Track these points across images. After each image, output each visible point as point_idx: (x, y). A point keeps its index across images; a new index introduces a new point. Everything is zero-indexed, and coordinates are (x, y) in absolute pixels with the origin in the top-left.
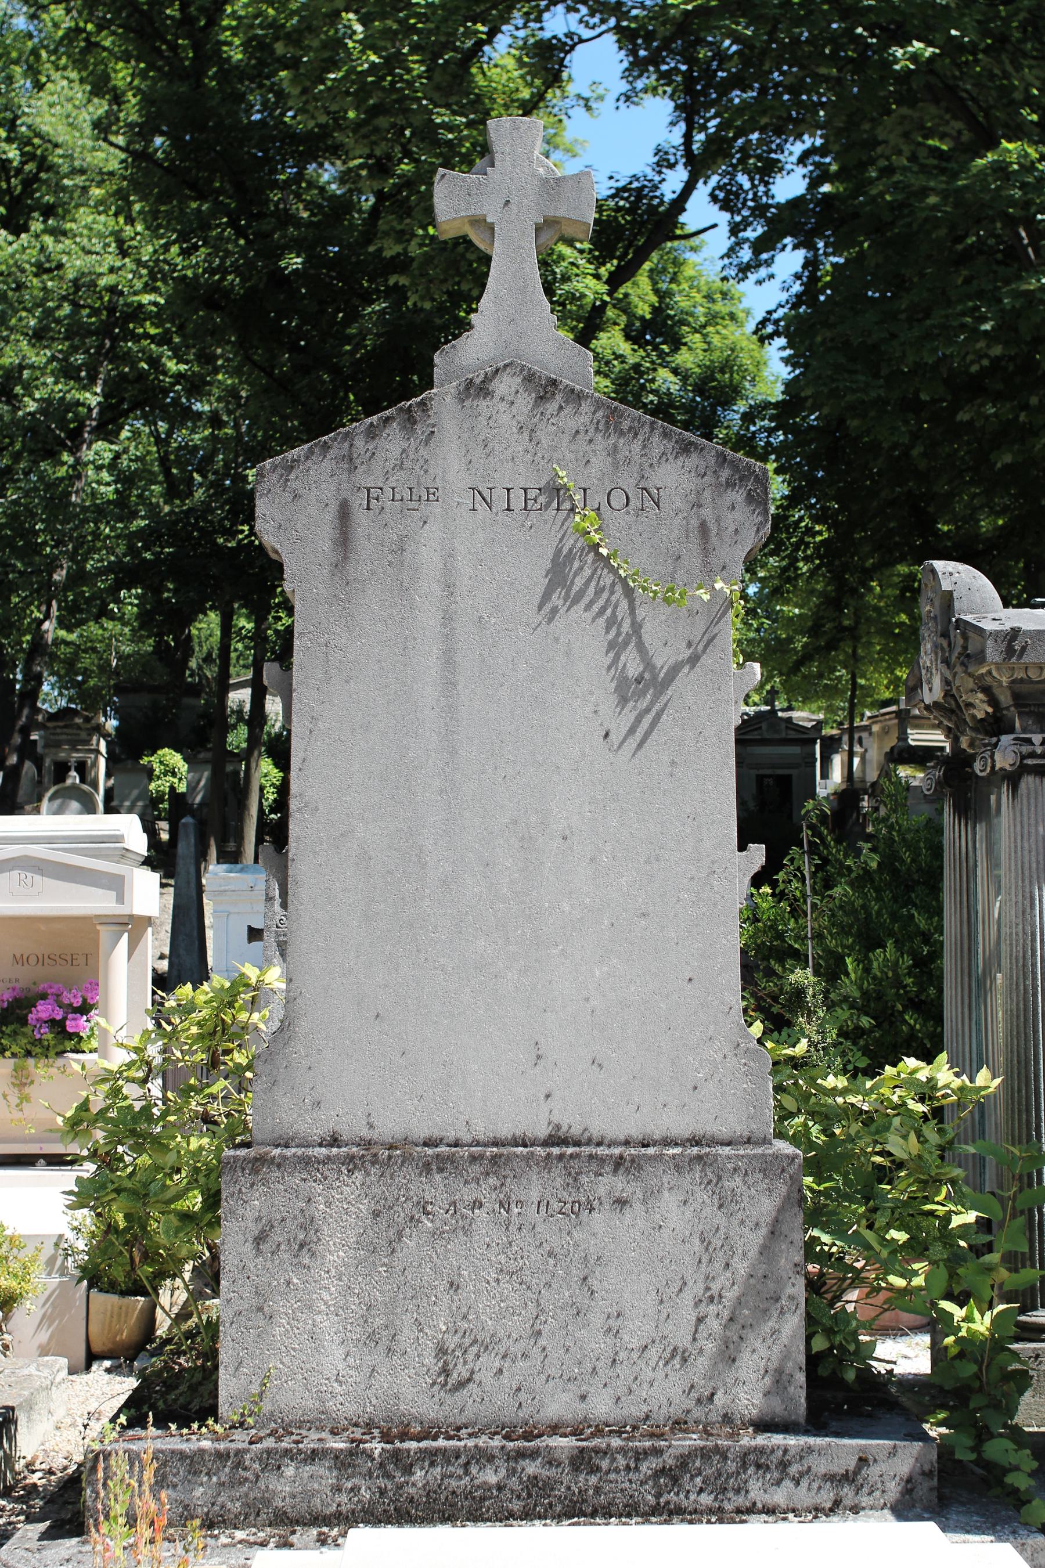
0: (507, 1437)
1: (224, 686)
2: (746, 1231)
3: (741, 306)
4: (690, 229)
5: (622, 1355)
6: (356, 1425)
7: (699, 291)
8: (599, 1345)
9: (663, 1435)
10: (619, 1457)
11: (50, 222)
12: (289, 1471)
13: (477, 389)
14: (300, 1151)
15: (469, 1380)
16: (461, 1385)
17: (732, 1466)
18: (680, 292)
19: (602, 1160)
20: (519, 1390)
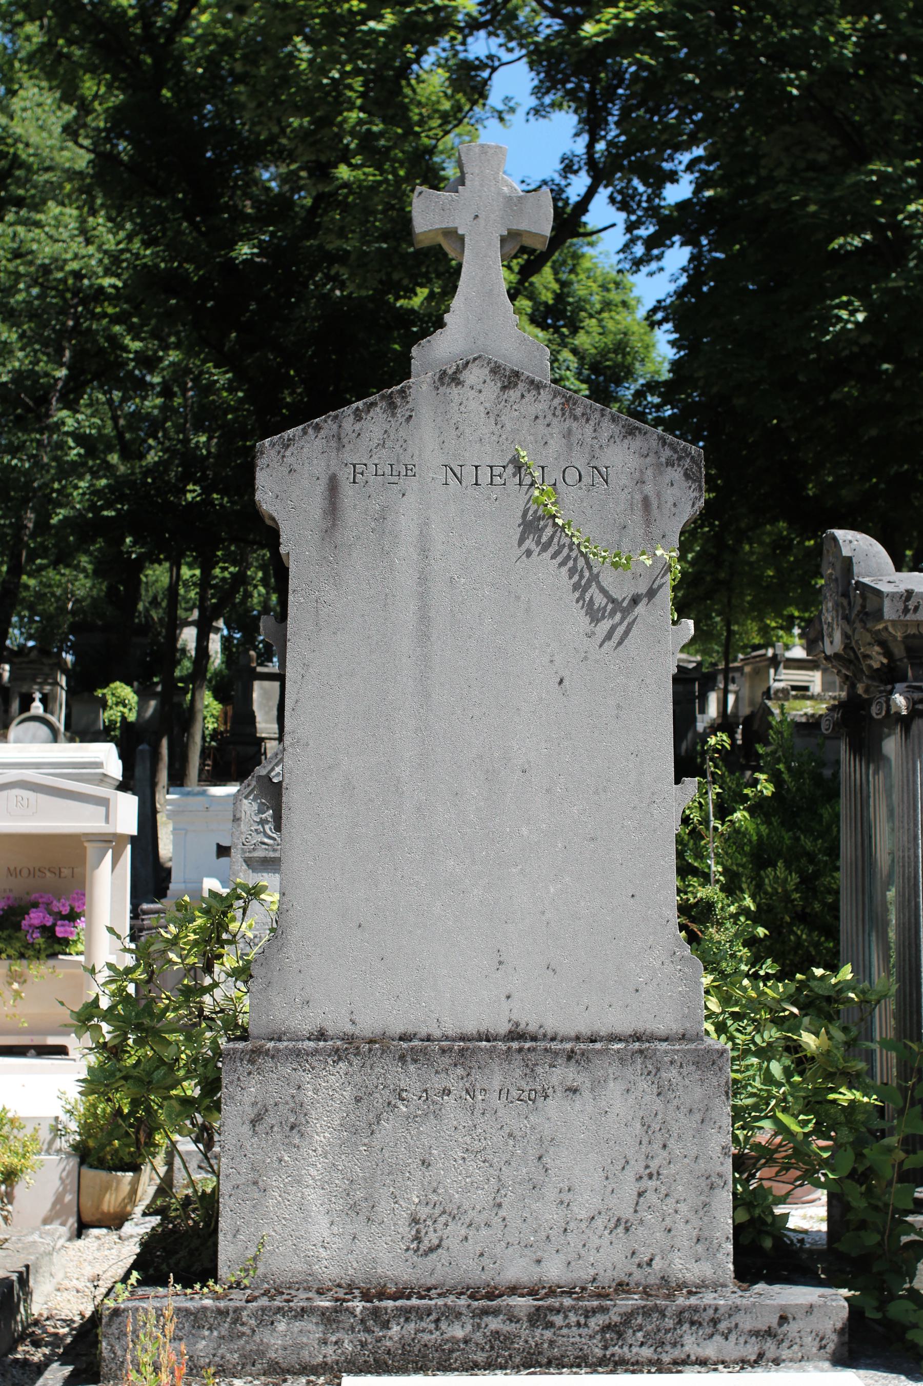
0: (472, 1297)
1: (174, 625)
2: (681, 1116)
3: (632, 295)
4: (590, 228)
5: (572, 1225)
6: (339, 1286)
7: (594, 282)
8: (552, 1215)
9: (608, 1295)
10: (571, 1314)
11: (22, 213)
12: (281, 1326)
13: (450, 378)
14: (291, 1045)
15: (439, 1246)
16: (432, 1250)
17: (669, 1323)
18: (579, 282)
19: (556, 1053)
20: (482, 1255)
